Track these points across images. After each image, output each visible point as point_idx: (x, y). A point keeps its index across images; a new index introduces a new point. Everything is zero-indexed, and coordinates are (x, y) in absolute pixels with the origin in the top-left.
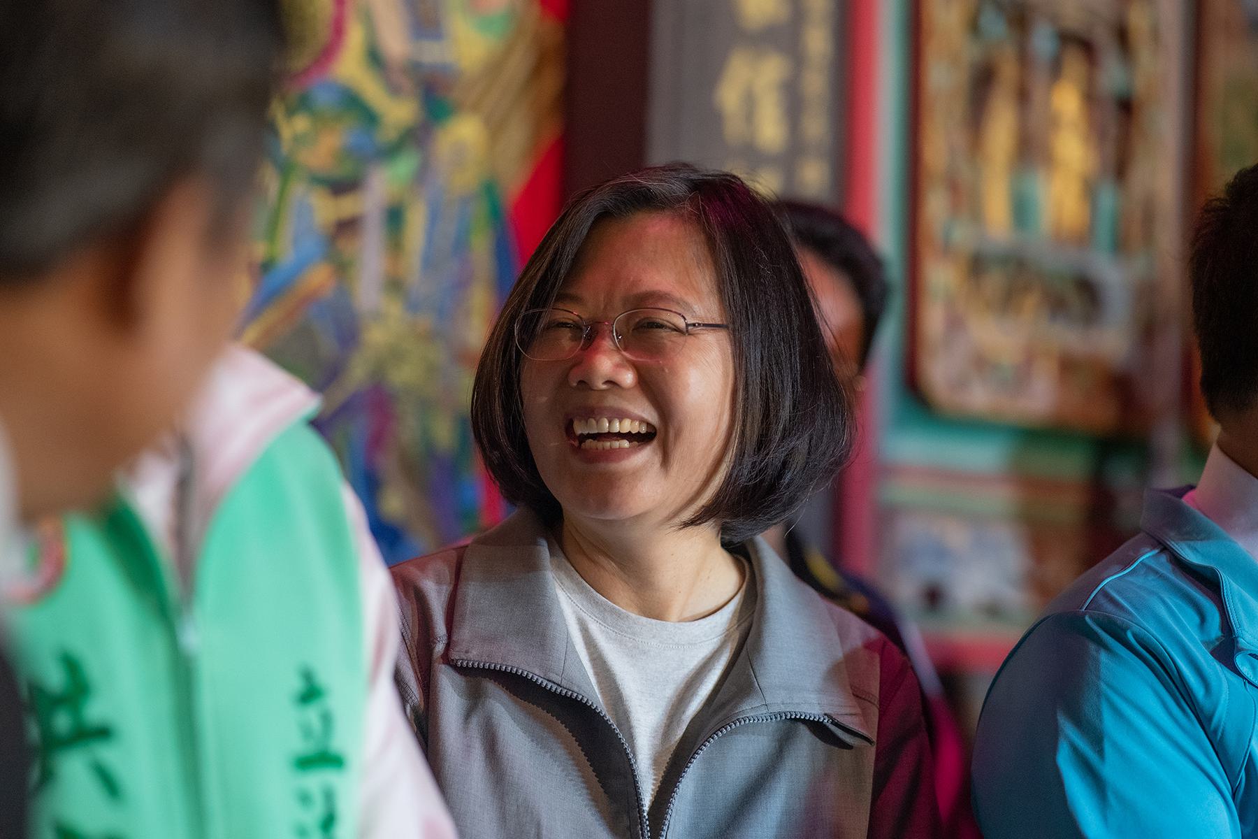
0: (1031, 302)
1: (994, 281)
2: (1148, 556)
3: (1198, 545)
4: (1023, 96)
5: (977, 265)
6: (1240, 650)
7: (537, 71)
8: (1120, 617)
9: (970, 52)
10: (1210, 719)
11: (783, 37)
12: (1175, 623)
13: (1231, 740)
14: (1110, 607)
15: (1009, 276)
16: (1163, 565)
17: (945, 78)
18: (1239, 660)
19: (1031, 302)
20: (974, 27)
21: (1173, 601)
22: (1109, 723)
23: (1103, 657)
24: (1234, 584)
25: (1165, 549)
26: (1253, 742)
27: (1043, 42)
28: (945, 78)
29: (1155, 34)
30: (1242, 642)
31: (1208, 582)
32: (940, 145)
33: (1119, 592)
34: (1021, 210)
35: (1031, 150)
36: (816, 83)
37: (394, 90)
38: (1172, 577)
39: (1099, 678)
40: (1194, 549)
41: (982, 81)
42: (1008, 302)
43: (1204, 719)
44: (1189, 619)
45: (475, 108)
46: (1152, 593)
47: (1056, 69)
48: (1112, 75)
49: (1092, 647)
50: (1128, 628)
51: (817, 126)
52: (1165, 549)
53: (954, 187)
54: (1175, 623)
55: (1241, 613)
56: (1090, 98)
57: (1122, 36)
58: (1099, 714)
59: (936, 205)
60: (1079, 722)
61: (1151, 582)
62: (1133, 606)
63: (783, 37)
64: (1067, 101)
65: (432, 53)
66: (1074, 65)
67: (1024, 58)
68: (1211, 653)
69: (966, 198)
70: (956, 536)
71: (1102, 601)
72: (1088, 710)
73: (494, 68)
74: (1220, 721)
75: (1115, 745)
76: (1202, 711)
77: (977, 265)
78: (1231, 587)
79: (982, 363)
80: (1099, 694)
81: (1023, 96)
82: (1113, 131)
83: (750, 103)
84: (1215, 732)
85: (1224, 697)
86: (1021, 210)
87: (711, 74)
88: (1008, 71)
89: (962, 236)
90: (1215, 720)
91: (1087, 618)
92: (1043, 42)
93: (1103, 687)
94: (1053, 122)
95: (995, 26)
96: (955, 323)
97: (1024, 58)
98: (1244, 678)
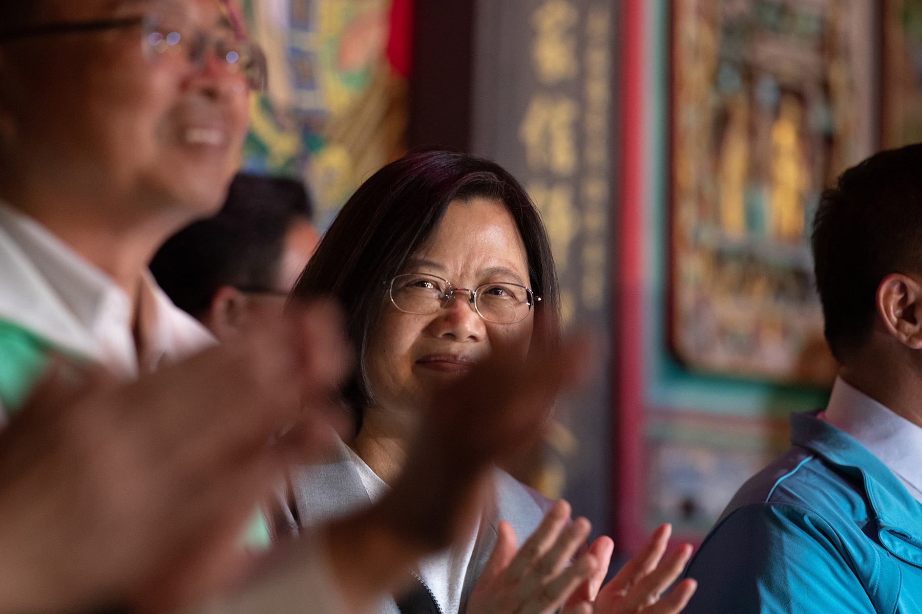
0: (760, 287)
1: (732, 269)
2: (806, 461)
3: (842, 452)
4: (752, 132)
5: (719, 259)
6: (882, 527)
7: (388, 114)
8: (797, 506)
9: (712, 100)
10: (868, 580)
11: (572, 88)
12: (829, 504)
13: (884, 596)
14: (787, 499)
15: (741, 266)
16: (818, 466)
17: (693, 118)
18: (883, 536)
19: (760, 287)
20: (715, 80)
21: (833, 494)
22: (793, 587)
23: (785, 538)
24: (874, 481)
25: (817, 456)
26: (900, 599)
27: (766, 92)
28: (693, 118)
29: (851, 86)
30: (882, 522)
31: (853, 479)
32: (691, 168)
33: (791, 488)
34: (752, 217)
35: (759, 173)
36: (597, 123)
37: (280, 128)
38: (831, 479)
39: (783, 553)
40: (839, 456)
41: (721, 123)
42: (742, 286)
43: (864, 581)
44: (845, 507)
45: (341, 141)
46: (814, 488)
47: (776, 113)
48: (818, 116)
49: (771, 525)
50: (804, 514)
51: (598, 155)
52: (817, 456)
53: (701, 199)
54: (829, 504)
55: (879, 500)
56: (803, 135)
57: (826, 88)
58: (786, 581)
59: (688, 214)
60: (770, 586)
61: (813, 480)
62: (804, 497)
63: (572, 88)
64: (785, 136)
65: (309, 101)
66: (790, 110)
67: (752, 102)
68: (863, 530)
69: (710, 209)
70: (705, 462)
71: (780, 494)
72: (776, 578)
73: (356, 112)
74: (875, 582)
75: (799, 604)
76: (861, 574)
77: (719, 259)
78: (872, 483)
79: (724, 332)
80: (784, 565)
81: (752, 132)
82: (819, 159)
83: (547, 138)
84: (872, 588)
85: (878, 563)
86: (752, 217)
87: (517, 116)
88: (740, 115)
89: (708, 236)
90: (871, 581)
91: (773, 509)
92: (766, 92)
93: (787, 560)
94: (775, 152)
95: (733, 82)
96: (703, 302)
97: (752, 102)
98: (886, 549)
